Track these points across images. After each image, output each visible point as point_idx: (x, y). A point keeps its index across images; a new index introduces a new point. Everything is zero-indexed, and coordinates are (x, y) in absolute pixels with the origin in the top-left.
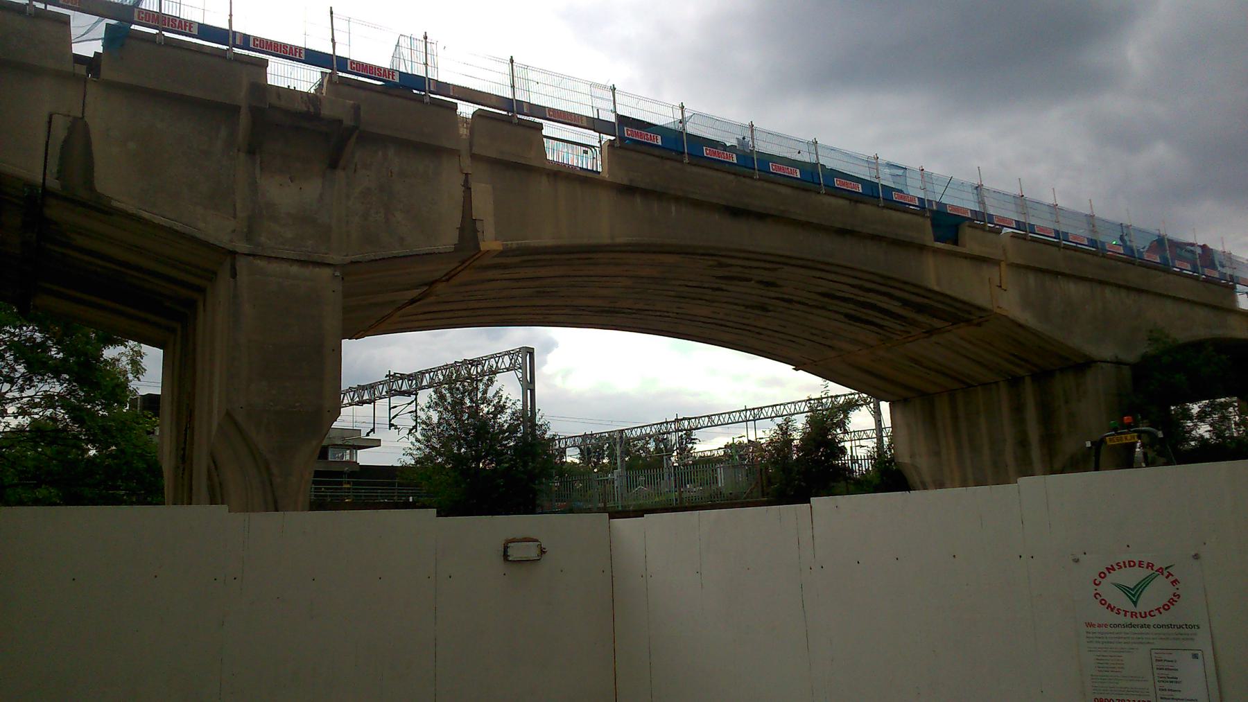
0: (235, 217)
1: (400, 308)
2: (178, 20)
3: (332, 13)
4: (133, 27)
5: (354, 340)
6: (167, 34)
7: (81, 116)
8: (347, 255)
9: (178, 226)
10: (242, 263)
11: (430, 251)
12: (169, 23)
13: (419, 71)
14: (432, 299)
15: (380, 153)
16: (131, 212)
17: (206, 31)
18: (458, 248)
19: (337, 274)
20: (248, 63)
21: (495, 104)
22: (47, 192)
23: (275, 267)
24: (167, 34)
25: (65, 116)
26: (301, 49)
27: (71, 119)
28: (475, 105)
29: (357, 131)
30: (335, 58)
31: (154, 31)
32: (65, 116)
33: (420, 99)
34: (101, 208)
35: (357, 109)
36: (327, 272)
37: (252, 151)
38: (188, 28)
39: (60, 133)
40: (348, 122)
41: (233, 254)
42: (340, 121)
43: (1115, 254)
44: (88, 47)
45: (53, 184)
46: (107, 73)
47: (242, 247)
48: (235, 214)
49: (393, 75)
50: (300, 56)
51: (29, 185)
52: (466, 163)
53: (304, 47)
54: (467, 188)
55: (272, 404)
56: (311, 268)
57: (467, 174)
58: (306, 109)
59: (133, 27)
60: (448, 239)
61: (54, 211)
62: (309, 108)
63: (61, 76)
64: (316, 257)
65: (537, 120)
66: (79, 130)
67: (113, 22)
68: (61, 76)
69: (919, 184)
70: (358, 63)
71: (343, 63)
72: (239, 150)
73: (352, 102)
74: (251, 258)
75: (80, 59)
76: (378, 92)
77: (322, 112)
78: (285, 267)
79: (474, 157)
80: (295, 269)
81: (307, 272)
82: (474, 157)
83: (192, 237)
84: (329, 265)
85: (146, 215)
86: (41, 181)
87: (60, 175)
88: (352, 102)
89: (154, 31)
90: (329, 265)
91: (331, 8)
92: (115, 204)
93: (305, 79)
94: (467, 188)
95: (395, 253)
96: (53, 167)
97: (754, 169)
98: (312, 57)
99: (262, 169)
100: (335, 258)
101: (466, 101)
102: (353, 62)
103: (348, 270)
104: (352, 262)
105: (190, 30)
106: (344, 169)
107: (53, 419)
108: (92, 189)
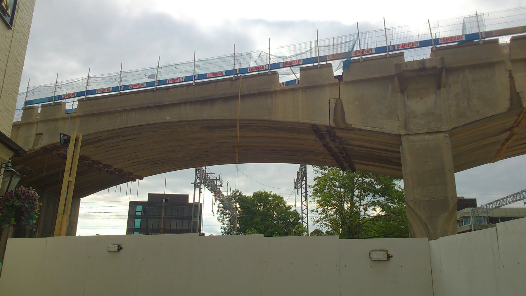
0: (399, 121)
1: (503, 145)
2: (367, 50)
3: (429, 22)
4: (352, 59)
5: (493, 163)
6: (363, 57)
7: (339, 97)
8: (450, 126)
9: (377, 129)
10: (404, 139)
11: (494, 114)
12: (364, 52)
13: (475, 31)
14: (514, 138)
15: (461, 75)
16: (359, 128)
17: (378, 50)
18: (509, 110)
19: (447, 135)
20: (395, 56)
21: (48, 101)
22: (332, 128)
23: (418, 138)
24: (363, 57)
25: (334, 99)
26: (417, 42)
27: (336, 99)
28: (510, 36)
29: (444, 69)
30: (433, 41)
31: (359, 57)
32: (334, 99)
33: (478, 43)
34: (350, 129)
35: (442, 59)
36: (442, 135)
37: (402, 92)
38: (461, 38)
39: (333, 105)
40: (439, 66)
41: (400, 136)
42: (436, 67)
43: (260, 72)
44: (338, 72)
45: (333, 124)
46: (345, 79)
47: (403, 132)
48: (399, 119)
49: (417, 44)
50: (417, 45)
51: (326, 127)
52: (509, 66)
53: (418, 41)
54: (511, 77)
55: (424, 197)
56: (434, 135)
57: (510, 71)
58: (419, 67)
59: (352, 59)
60: (504, 105)
61: (339, 134)
62: (420, 66)
63: (332, 85)
64: (436, 130)
65: (328, 62)
66: (339, 102)
67: (345, 60)
68: (332, 85)
69: (161, 74)
70: (400, 45)
71: (436, 41)
72: (397, 93)
73: (439, 57)
74: (408, 136)
75: (336, 77)
76: (457, 47)
77: (426, 66)
78: (422, 136)
79: (513, 61)
80: (427, 137)
81: (432, 137)
82: (513, 61)
83: (383, 132)
84: (442, 132)
85: (364, 128)
86: (329, 124)
87: (335, 121)
88: (439, 57)
89: (359, 57)
90: (442, 132)
91: (428, 20)
92: (353, 126)
93: (425, 53)
94: (511, 77)
95: (475, 119)
96: (332, 118)
97: (54, 101)
98: (423, 44)
99: (408, 97)
100: (445, 128)
101: (90, 95)
102: (441, 39)
103: (452, 133)
104: (453, 128)
105: (462, 39)
106: (445, 87)
107: (32, 218)
108: (345, 123)
